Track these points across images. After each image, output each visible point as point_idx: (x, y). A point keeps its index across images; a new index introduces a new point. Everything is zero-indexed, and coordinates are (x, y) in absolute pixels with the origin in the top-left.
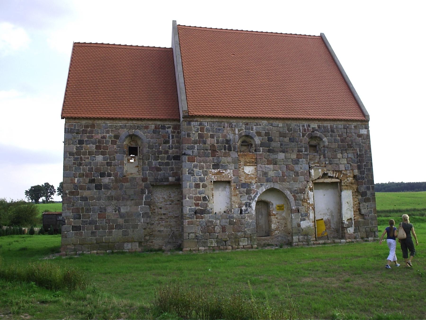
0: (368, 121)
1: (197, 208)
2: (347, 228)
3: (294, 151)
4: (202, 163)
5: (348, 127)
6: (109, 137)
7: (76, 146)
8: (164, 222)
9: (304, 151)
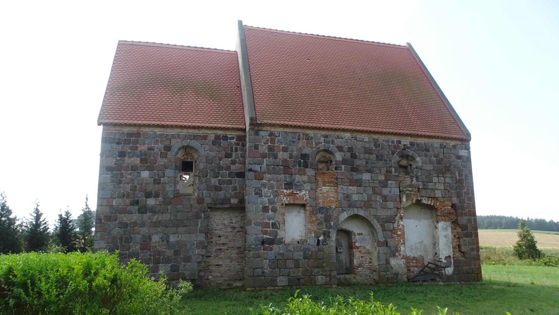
0: (469, 140)
1: (265, 236)
2: (444, 268)
3: (382, 171)
4: (272, 182)
5: (445, 146)
6: (158, 148)
7: (116, 159)
8: (223, 253)
9: (393, 171)
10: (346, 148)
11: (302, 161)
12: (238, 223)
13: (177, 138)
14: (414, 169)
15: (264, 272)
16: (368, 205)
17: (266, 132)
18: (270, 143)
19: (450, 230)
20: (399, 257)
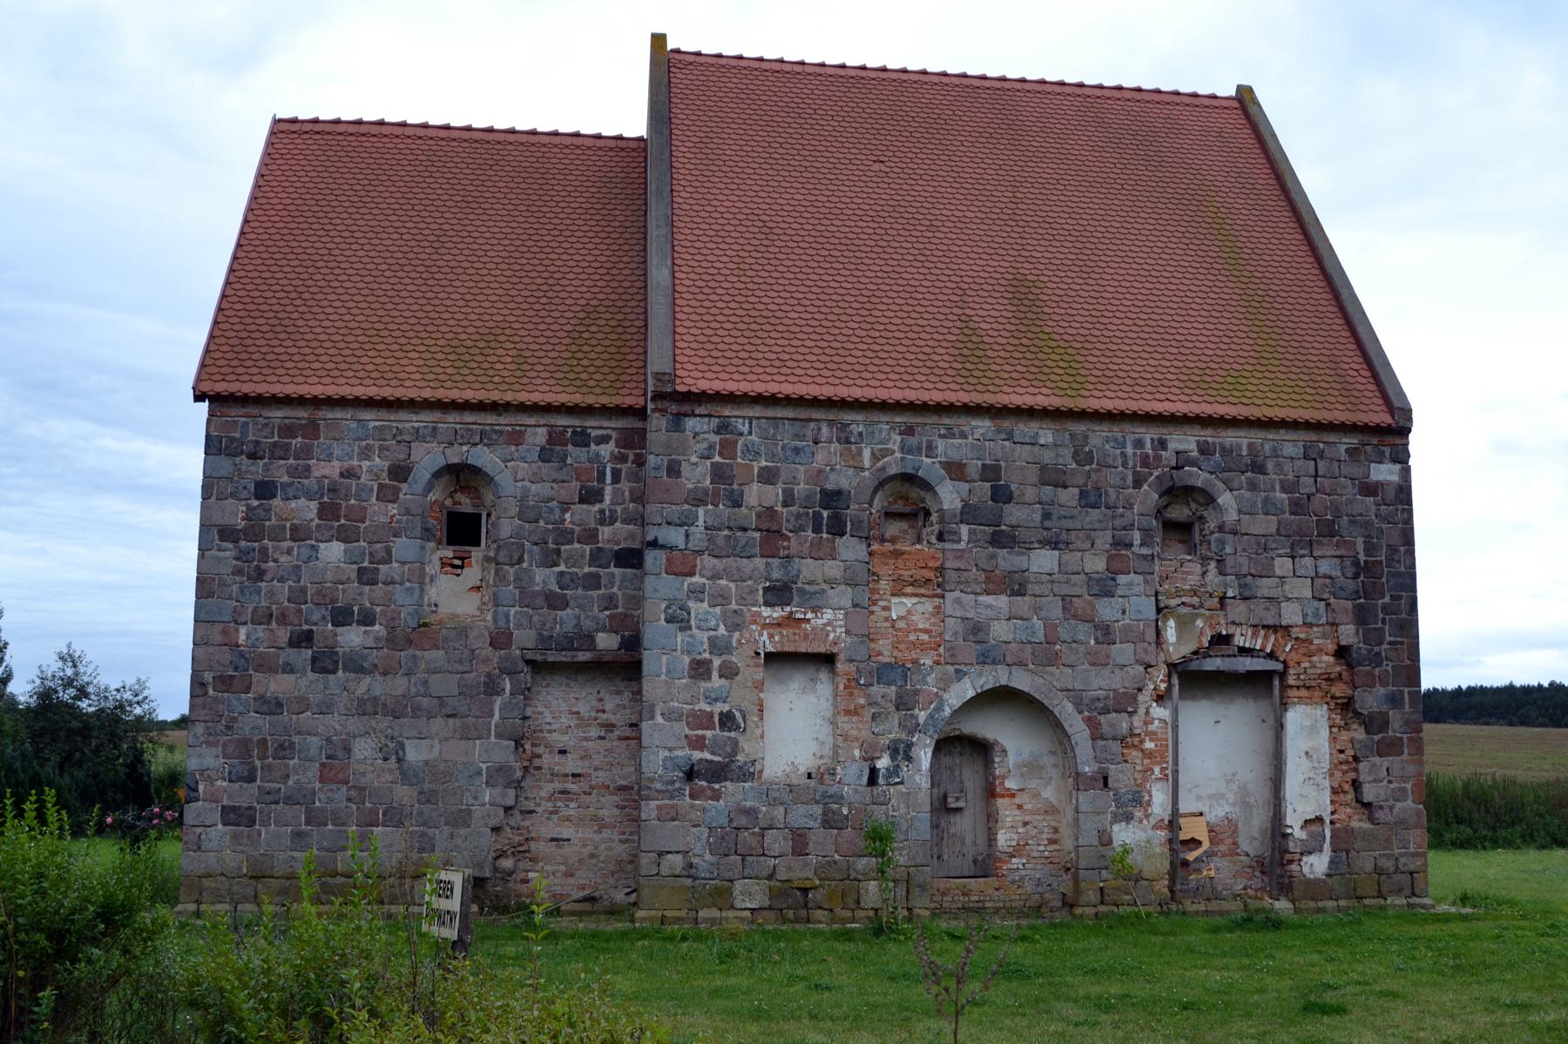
0: (1404, 431)
4: (723, 582)
7: (247, 505)
8: (572, 805)
9: (1137, 542)
10: (974, 468)
11: (825, 514)
12: (623, 712)
13: (428, 439)
14: (1212, 533)
15: (691, 865)
16: (1047, 655)
17: (706, 420)
18: (721, 454)
19: (1325, 733)
20: (1145, 822)
